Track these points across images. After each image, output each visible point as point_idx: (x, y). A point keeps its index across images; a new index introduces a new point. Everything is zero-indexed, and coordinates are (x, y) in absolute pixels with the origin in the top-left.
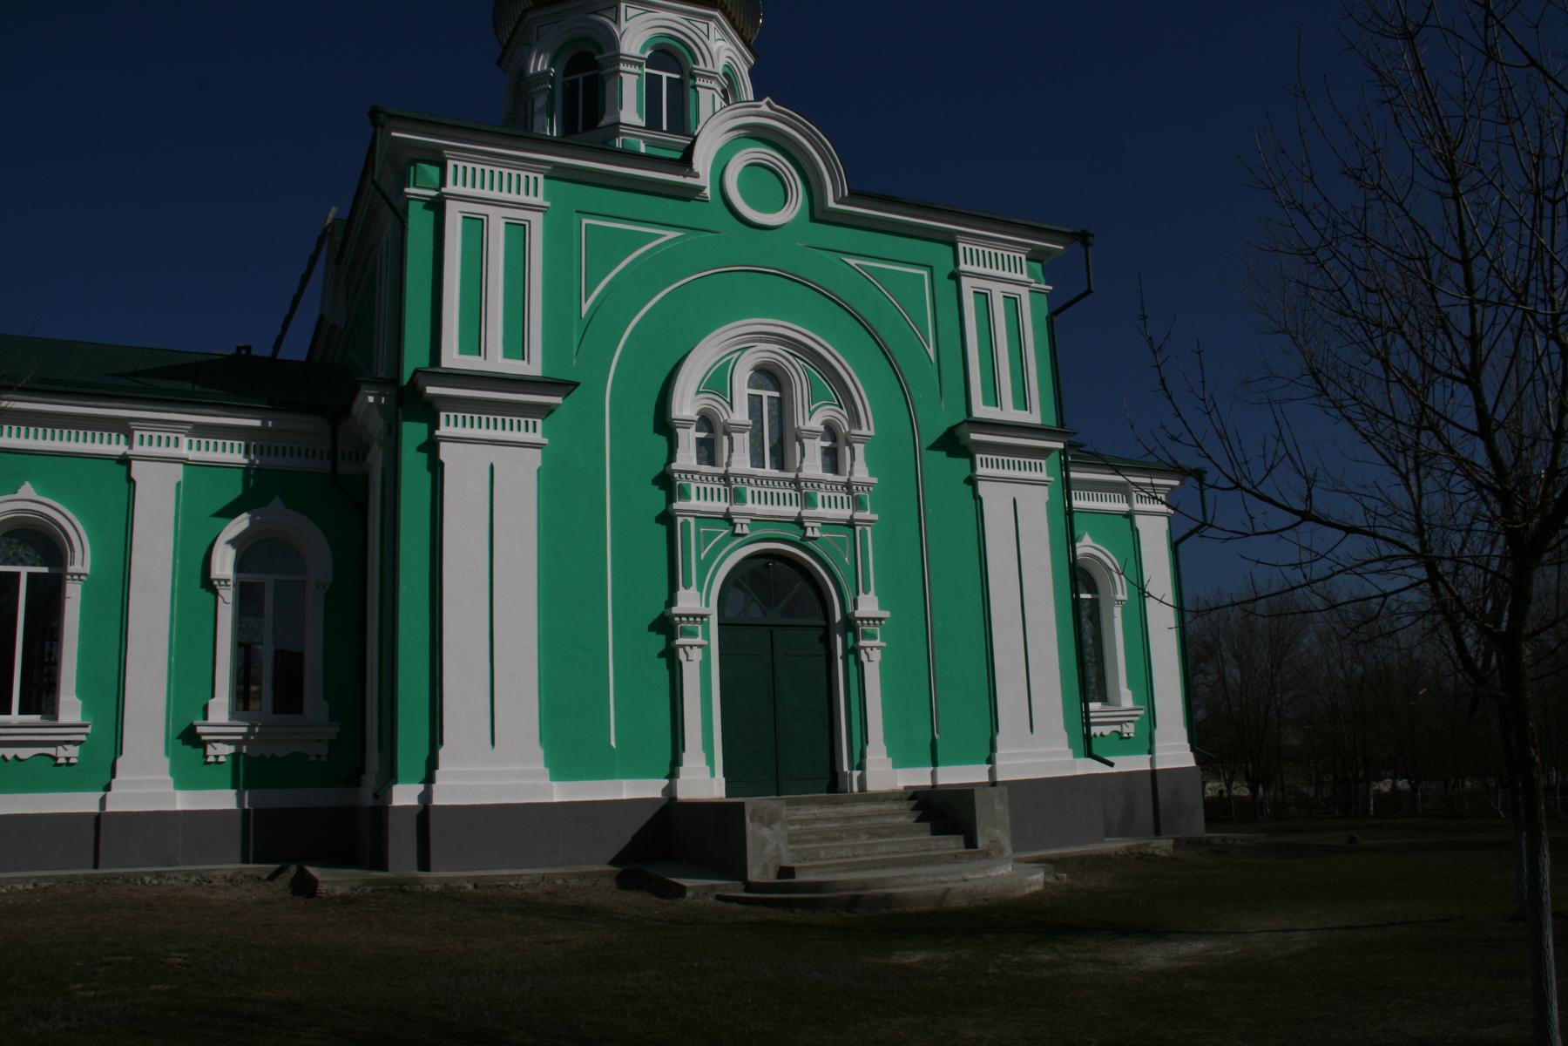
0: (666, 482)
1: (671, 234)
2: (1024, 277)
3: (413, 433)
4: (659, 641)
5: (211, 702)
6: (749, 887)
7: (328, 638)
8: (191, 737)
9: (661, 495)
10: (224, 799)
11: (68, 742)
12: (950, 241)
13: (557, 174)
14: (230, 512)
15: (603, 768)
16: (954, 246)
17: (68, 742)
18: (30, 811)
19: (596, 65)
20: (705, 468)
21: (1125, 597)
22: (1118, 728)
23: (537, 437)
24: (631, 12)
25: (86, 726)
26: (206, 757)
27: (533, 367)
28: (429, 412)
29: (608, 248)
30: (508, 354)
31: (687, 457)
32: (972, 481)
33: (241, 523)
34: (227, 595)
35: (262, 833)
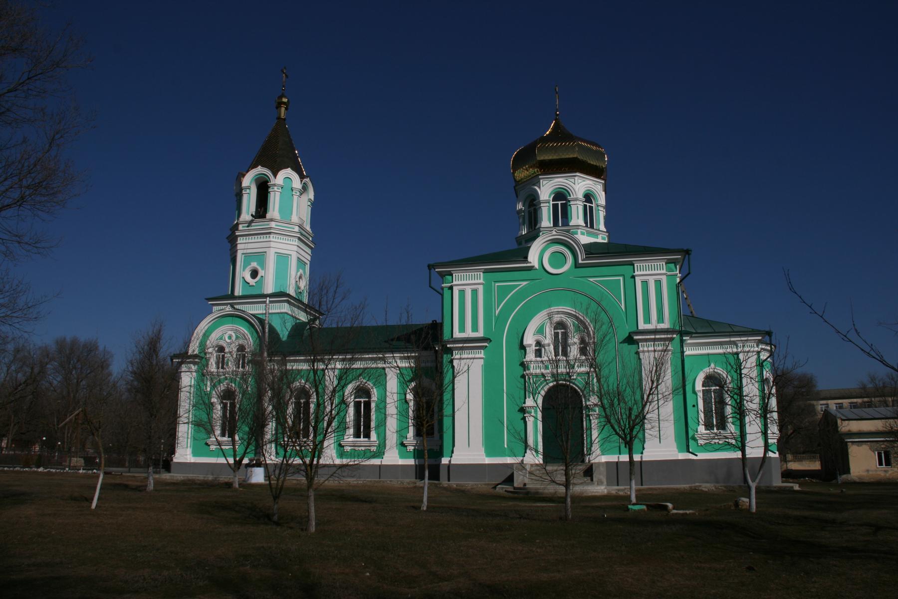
0: (524, 366)
1: (525, 283)
2: (664, 271)
3: (446, 358)
4: (521, 415)
6: (515, 488)
7: (430, 417)
8: (403, 444)
9: (521, 368)
10: (411, 462)
12: (632, 264)
13: (486, 271)
14: (411, 381)
15: (502, 454)
16: (633, 265)
19: (535, 205)
20: (538, 359)
23: (482, 355)
24: (545, 182)
27: (480, 334)
28: (450, 351)
29: (504, 291)
30: (473, 331)
31: (531, 356)
32: (637, 353)
33: (413, 384)
35: (419, 471)
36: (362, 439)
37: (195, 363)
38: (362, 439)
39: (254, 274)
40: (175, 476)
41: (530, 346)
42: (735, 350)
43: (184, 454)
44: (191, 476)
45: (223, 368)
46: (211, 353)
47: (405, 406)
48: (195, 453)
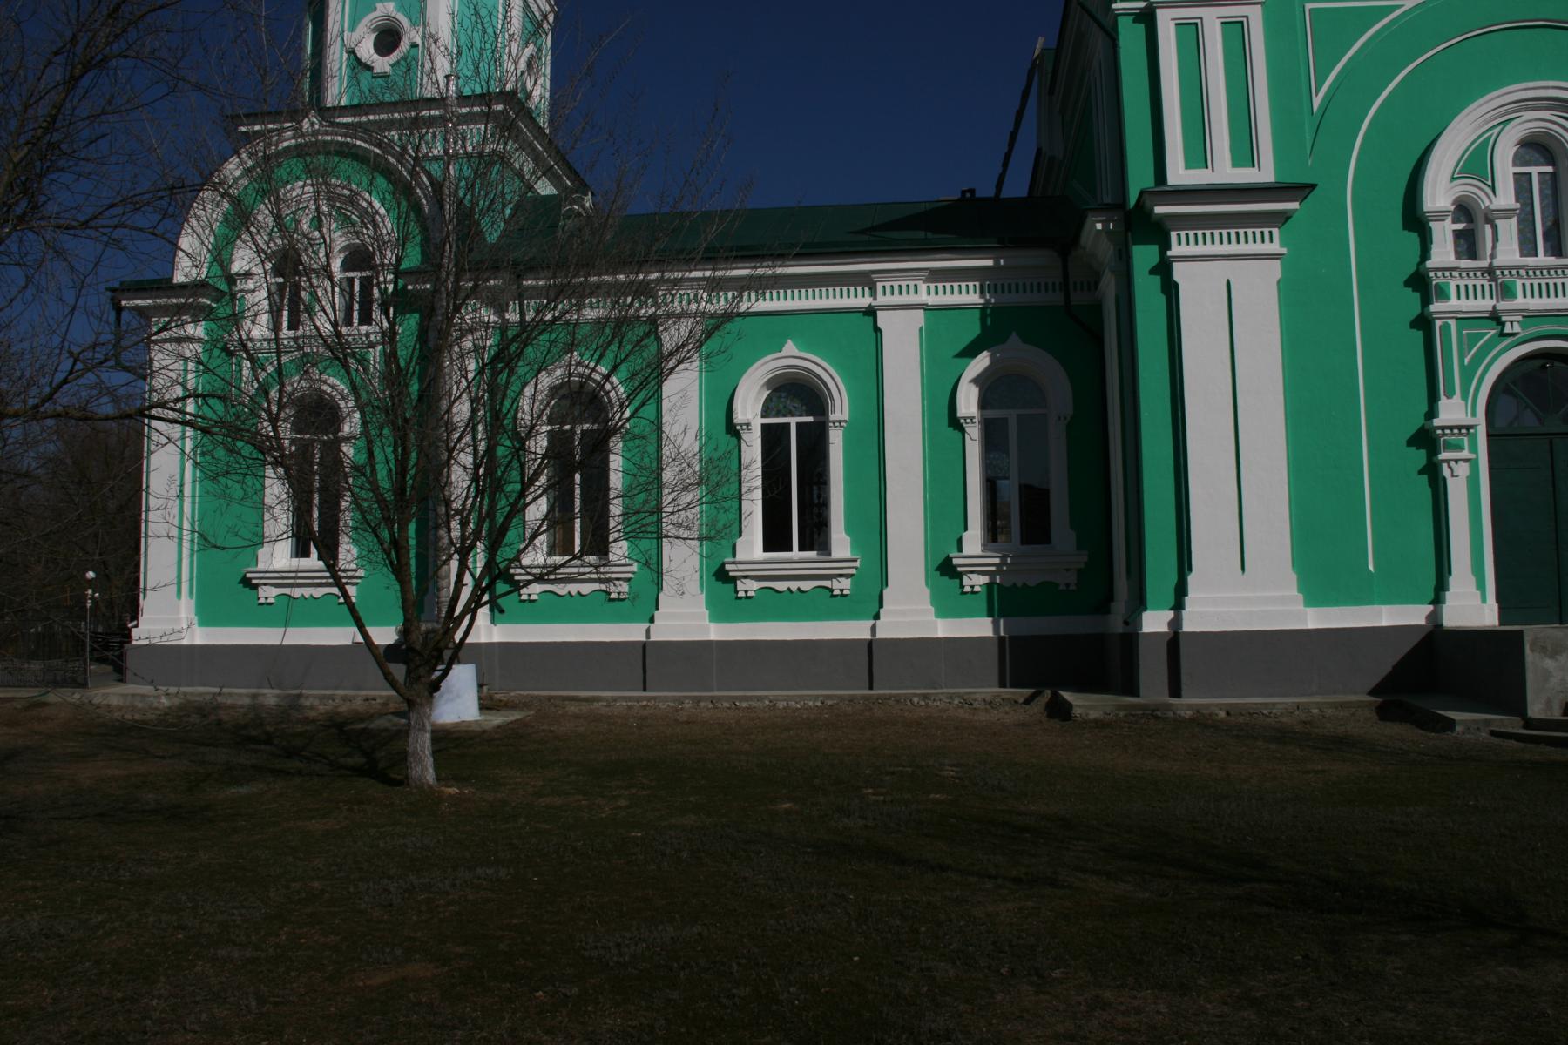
0: (1421, 283)
3: (1144, 256)
5: (965, 535)
6: (1529, 723)
7: (1075, 471)
10: (981, 627)
14: (970, 352)
15: (1361, 592)
20: (1466, 263)
23: (1275, 247)
26: (962, 587)
27: (1265, 174)
28: (1159, 233)
31: (1443, 252)
33: (982, 361)
34: (974, 432)
35: (1020, 660)
36: (796, 553)
37: (200, 314)
38: (796, 553)
39: (388, 38)
40: (113, 696)
41: (1440, 215)
42: (865, 301)
43: (169, 616)
44: (200, 691)
45: (293, 325)
46: (248, 275)
47: (726, 441)
48: (208, 614)
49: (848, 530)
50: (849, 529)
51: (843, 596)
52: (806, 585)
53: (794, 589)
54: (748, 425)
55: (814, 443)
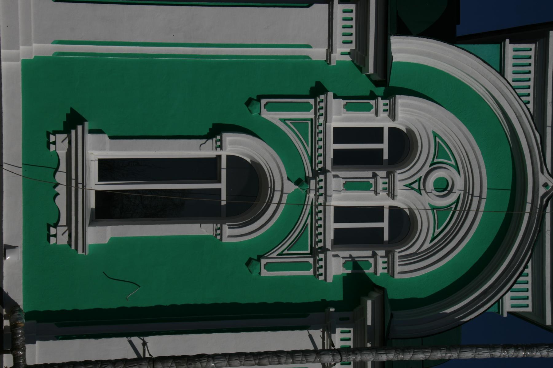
5: (106, 137)
11: (70, 143)
17: (70, 143)
18: (4, 151)
21: (225, 240)
22: (63, 221)
23: (337, 57)
25: (84, 250)
26: (55, 133)
34: (202, 150)
49: (114, 241)
50: (115, 242)
51: (49, 144)
52: (61, 202)
53: (57, 189)
54: (221, 147)
55: (201, 208)
